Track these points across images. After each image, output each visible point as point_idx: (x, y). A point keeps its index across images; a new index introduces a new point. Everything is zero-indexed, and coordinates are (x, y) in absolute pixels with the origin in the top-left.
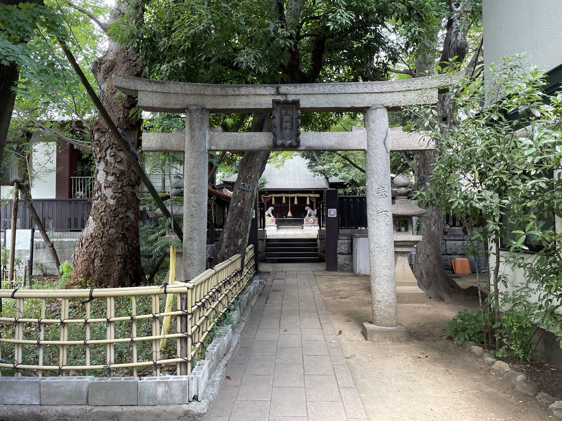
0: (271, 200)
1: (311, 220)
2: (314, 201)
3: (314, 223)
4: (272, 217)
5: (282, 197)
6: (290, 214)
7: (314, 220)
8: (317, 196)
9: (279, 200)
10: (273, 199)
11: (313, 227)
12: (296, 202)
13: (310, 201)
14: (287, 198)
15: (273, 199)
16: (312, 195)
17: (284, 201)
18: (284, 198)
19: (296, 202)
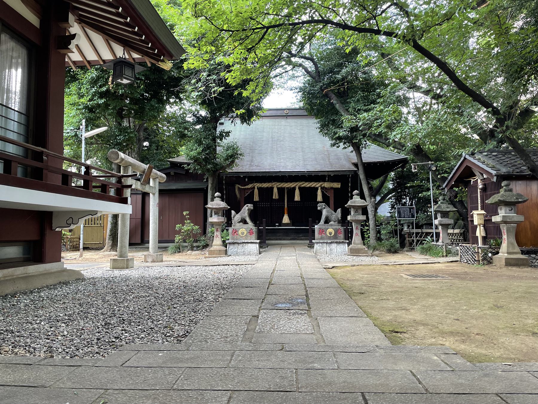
0: (252, 193)
1: (330, 230)
2: (331, 195)
3: (335, 237)
4: (250, 225)
5: (272, 188)
6: (286, 219)
7: (336, 231)
8: (337, 185)
9: (266, 193)
10: (256, 191)
11: (334, 246)
12: (297, 198)
14: (281, 191)
15: (256, 191)
16: (326, 185)
17: (275, 196)
18: (275, 190)
19: (297, 198)
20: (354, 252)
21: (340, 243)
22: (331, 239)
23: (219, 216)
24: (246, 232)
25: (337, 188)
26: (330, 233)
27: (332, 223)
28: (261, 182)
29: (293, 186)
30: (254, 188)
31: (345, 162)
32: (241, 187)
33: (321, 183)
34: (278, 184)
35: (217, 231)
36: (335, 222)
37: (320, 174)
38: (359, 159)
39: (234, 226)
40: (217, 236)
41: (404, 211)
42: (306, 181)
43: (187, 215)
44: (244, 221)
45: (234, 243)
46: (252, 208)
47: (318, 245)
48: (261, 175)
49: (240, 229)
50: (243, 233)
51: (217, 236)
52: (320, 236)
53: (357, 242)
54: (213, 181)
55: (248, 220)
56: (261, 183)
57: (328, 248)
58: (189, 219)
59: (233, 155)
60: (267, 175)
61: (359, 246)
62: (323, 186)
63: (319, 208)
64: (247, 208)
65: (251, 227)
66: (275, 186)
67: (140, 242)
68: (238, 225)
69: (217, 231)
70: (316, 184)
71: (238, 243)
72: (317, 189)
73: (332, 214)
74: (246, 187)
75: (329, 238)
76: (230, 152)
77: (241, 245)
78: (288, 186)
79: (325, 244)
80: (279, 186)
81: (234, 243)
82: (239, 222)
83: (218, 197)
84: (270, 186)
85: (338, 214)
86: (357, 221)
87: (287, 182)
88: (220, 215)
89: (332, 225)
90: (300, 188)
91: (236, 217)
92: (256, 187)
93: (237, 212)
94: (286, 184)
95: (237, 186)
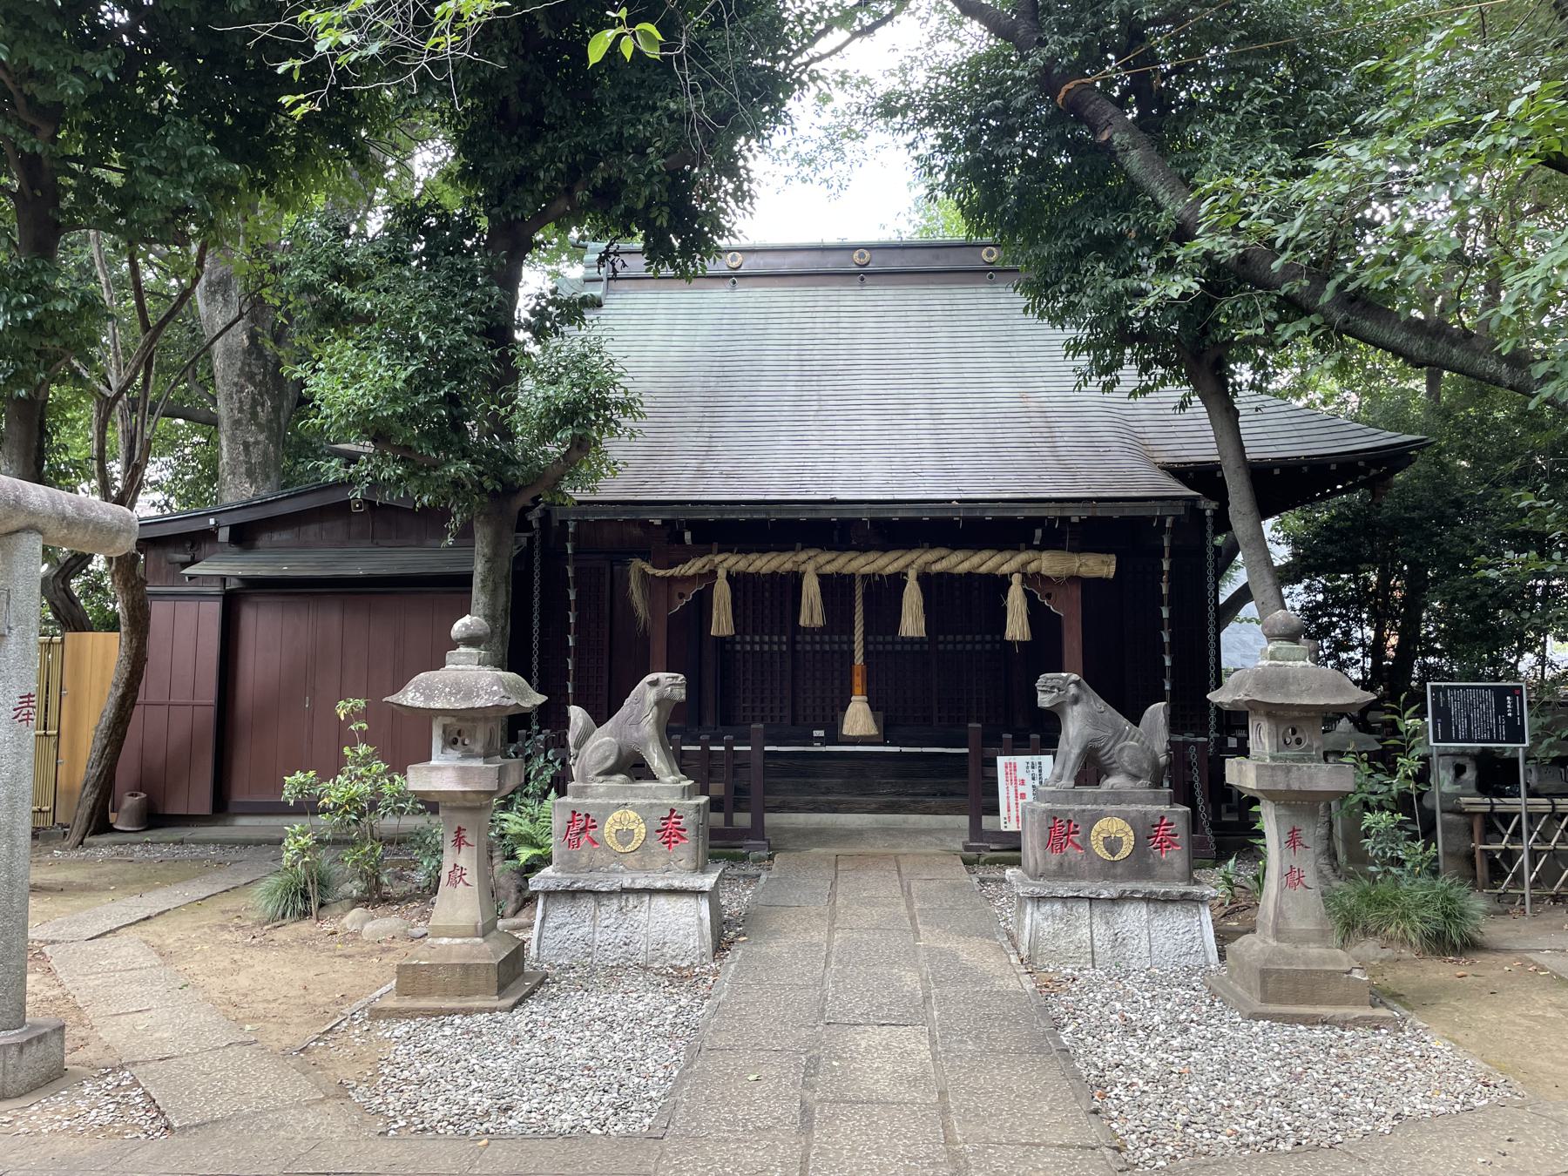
0: (703, 602)
1: (1113, 826)
2: (1069, 611)
3: (1140, 865)
4: (669, 788)
5: (796, 579)
6: (858, 718)
7: (1148, 833)
8: (1100, 566)
9: (767, 600)
10: (722, 592)
11: (1134, 917)
12: (912, 623)
13: (1036, 613)
14: (836, 588)
15: (722, 592)
16: (1049, 563)
17: (811, 612)
18: (811, 588)
19: (912, 623)
20: (1287, 993)
21: (1167, 900)
22: (1115, 878)
23: (469, 755)
24: (641, 831)
25: (1100, 581)
26: (1112, 845)
27: (1115, 782)
28: (745, 551)
29: (891, 569)
30: (713, 574)
31: (1127, 462)
32: (650, 571)
33: (1023, 557)
34: (824, 557)
35: (459, 841)
36: (1136, 777)
37: (1020, 515)
38: (1228, 440)
39: (580, 793)
40: (458, 875)
41: (1469, 707)
42: (955, 547)
43: (353, 716)
44: (633, 767)
45: (573, 894)
46: (680, 694)
47: (1046, 908)
48: (743, 517)
49: (608, 810)
50: (625, 836)
51: (458, 875)
52: (1055, 858)
53: (1297, 924)
54: (496, 543)
55: (656, 759)
56: (747, 552)
57: (1100, 929)
58: (365, 737)
59: (587, 414)
60: (774, 517)
61: (1314, 950)
62: (1032, 567)
63: (1044, 700)
64: (652, 695)
65: (674, 801)
66: (810, 568)
67: (206, 810)
68: (600, 786)
69: (459, 841)
70: (998, 558)
71: (596, 893)
72: (1003, 583)
73: (1119, 735)
74: (670, 572)
75: (1108, 871)
76: (564, 392)
77: (615, 904)
78: (867, 570)
79: (1083, 909)
80: (829, 569)
81: (573, 894)
82: (610, 772)
83: (471, 641)
84: (788, 566)
85: (1151, 732)
86: (1298, 803)
87: (863, 549)
88: (478, 748)
89: (1117, 797)
90: (925, 579)
91: (590, 745)
92: (722, 573)
93: (601, 714)
94: (862, 560)
95: (637, 564)
